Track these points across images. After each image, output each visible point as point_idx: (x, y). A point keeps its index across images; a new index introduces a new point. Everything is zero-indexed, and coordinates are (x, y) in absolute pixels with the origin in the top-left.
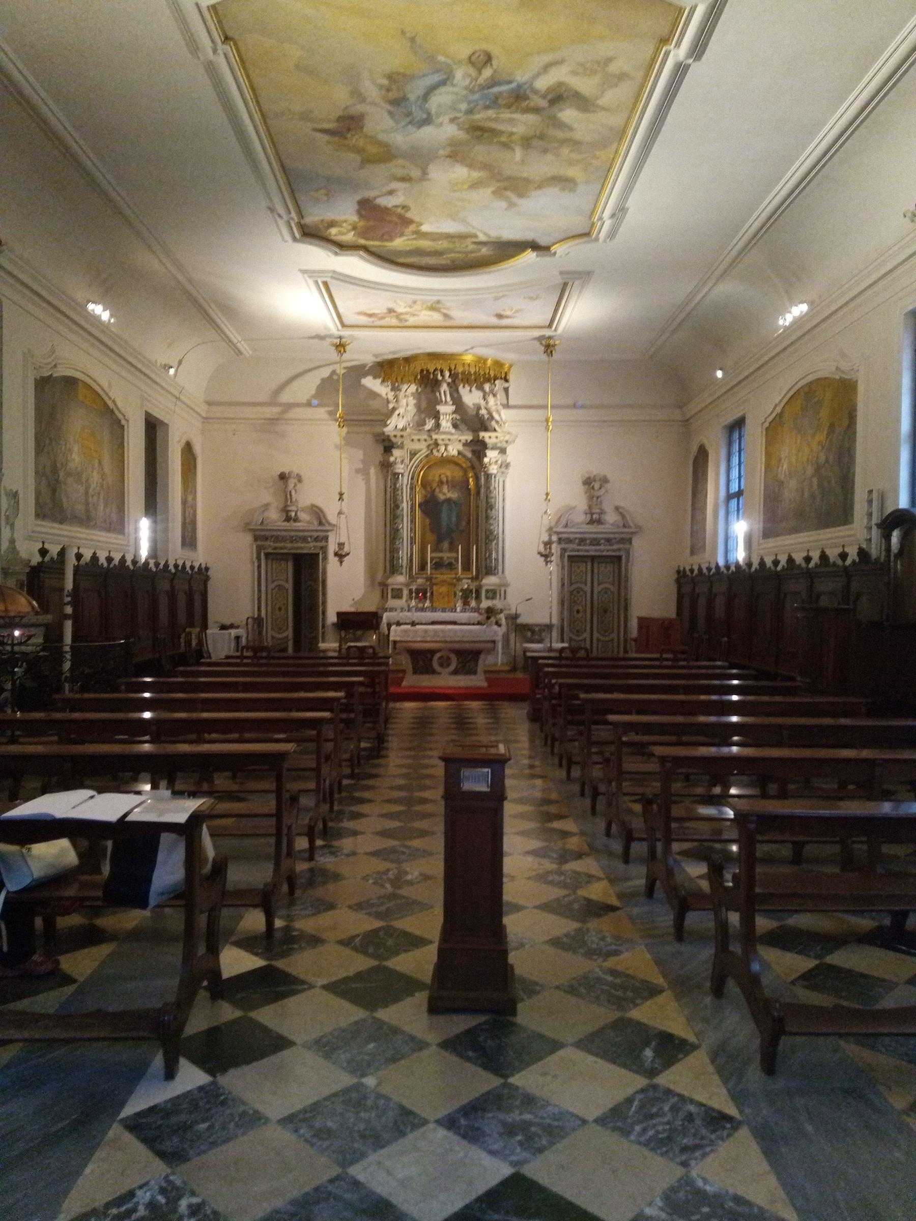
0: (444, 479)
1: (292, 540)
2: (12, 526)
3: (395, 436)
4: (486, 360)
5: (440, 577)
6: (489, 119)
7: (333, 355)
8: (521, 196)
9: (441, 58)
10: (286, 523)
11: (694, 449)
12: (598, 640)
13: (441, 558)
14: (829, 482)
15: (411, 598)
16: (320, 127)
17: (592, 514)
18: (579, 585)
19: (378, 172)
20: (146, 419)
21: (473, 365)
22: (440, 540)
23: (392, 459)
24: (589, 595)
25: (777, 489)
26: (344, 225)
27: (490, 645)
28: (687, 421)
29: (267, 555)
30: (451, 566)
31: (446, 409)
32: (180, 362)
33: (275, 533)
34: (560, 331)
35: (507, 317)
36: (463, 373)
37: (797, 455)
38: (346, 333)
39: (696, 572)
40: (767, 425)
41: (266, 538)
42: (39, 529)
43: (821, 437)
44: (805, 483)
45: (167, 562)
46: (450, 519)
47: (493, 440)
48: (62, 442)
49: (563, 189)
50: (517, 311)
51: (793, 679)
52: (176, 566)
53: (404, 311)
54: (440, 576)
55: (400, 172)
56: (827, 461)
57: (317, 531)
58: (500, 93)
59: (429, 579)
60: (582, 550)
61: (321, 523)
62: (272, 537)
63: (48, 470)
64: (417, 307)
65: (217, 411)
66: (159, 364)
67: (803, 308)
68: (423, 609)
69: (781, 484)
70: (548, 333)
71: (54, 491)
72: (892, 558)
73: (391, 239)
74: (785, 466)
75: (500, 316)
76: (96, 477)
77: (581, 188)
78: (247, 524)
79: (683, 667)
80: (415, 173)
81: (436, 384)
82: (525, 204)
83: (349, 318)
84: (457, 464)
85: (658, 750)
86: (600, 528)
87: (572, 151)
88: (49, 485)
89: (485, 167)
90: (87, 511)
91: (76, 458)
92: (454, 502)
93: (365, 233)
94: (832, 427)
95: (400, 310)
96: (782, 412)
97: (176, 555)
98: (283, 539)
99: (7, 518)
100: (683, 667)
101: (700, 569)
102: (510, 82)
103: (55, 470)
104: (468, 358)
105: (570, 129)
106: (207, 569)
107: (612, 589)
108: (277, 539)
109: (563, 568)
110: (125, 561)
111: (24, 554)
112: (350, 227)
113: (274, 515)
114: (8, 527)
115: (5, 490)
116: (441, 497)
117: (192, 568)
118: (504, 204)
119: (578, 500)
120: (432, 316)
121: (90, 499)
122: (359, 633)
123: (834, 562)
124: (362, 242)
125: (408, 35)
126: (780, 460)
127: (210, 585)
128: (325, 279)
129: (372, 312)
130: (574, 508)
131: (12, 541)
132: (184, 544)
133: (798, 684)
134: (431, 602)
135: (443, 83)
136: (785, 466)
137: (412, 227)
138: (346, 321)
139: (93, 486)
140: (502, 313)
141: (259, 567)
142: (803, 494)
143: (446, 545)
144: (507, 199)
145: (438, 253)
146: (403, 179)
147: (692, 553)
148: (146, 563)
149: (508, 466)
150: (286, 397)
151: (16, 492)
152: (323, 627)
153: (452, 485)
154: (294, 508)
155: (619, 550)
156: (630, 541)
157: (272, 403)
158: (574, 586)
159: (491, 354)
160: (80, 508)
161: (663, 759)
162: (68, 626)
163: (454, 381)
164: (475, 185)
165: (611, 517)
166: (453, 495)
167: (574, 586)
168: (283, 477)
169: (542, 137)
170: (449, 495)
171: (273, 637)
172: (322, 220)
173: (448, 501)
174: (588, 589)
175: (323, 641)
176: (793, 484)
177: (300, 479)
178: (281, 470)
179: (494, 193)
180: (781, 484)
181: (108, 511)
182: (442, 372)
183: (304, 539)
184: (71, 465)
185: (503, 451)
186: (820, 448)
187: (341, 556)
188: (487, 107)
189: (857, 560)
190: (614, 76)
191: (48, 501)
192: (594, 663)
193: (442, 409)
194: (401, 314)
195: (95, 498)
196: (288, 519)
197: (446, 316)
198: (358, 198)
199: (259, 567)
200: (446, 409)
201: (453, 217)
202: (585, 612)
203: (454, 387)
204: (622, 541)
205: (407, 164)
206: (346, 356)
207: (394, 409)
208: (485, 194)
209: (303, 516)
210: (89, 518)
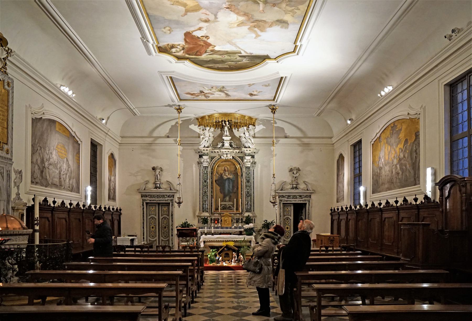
0: (227, 170)
2: (18, 187)
4: (245, 116)
5: (226, 213)
7: (176, 114)
10: (155, 189)
11: (337, 157)
13: (225, 205)
14: (406, 166)
15: (211, 223)
17: (293, 185)
18: (287, 216)
19: (193, 18)
20: (91, 142)
21: (239, 118)
22: (225, 197)
23: (202, 160)
25: (379, 171)
26: (178, 47)
27: (248, 244)
29: (147, 203)
30: (229, 208)
31: (227, 139)
32: (108, 118)
34: (278, 102)
35: (255, 95)
37: (389, 155)
38: (182, 103)
39: (340, 210)
40: (373, 142)
42: (32, 189)
43: (401, 146)
44: (394, 167)
45: (100, 206)
47: (248, 152)
48: (47, 149)
49: (282, 27)
50: (259, 92)
51: (399, 259)
52: (105, 208)
53: (207, 92)
54: (226, 213)
55: (204, 17)
56: (404, 157)
59: (220, 214)
60: (289, 201)
61: (171, 189)
62: (149, 195)
63: (39, 162)
64: (214, 90)
65: (125, 141)
66: (98, 118)
68: (217, 228)
69: (381, 169)
70: (273, 103)
71: (42, 172)
72: (444, 200)
73: (201, 55)
74: (383, 160)
75: (251, 95)
76: (65, 166)
77: (291, 27)
78: (138, 190)
79: (344, 254)
80: (211, 17)
81: (223, 127)
82: (264, 35)
83: (184, 96)
85: (316, 286)
86: (297, 191)
87: (287, 5)
88: (39, 169)
89: (245, 14)
90: (60, 182)
91: (54, 157)
92: (231, 179)
93: (188, 51)
94: (406, 141)
95: (205, 92)
96: (380, 136)
97: (105, 203)
98: (154, 196)
99: (15, 183)
100: (344, 254)
101: (342, 208)
103: (43, 162)
104: (237, 116)
106: (120, 210)
108: (151, 196)
109: (280, 209)
110: (79, 205)
111: (25, 201)
112: (181, 48)
113: (151, 186)
114: (16, 187)
115: (14, 169)
116: (225, 177)
117: (113, 209)
118: (254, 35)
119: (288, 178)
120: (220, 95)
121: (62, 176)
122: (188, 238)
123: (411, 203)
124: (187, 56)
126: (380, 158)
127: (122, 217)
128: (171, 76)
129: (193, 93)
130: (285, 182)
131: (18, 194)
132: (109, 198)
133: (401, 262)
134: (221, 224)
136: (383, 160)
137: (211, 48)
138: (182, 98)
139: (63, 170)
140: (252, 93)
141: (143, 209)
142: (392, 172)
143: (227, 198)
144: (255, 32)
145: (223, 62)
146: (207, 21)
147: (337, 202)
148: (90, 206)
149: (255, 163)
150: (155, 134)
151: (21, 171)
152: (172, 235)
153: (230, 173)
155: (305, 200)
156: (310, 196)
157: (150, 137)
159: (248, 113)
160: (56, 180)
161: (319, 290)
162: (37, 234)
163: (230, 126)
164: (241, 24)
165: (302, 186)
166: (231, 177)
168: (154, 169)
170: (229, 176)
171: (150, 240)
172: (168, 44)
173: (229, 179)
175: (313, 247)
176: (387, 168)
179: (249, 29)
180: (381, 169)
181: (71, 182)
182: (225, 122)
183: (163, 196)
184: (51, 160)
185: (253, 157)
186: (401, 151)
187: (179, 203)
189: (423, 201)
191: (39, 176)
194: (206, 93)
195: (64, 176)
196: (156, 188)
197: (227, 94)
198: (185, 32)
199: (143, 209)
201: (230, 42)
203: (230, 130)
204: (306, 196)
205: (208, 12)
206: (181, 115)
208: (245, 29)
209: (164, 186)
210: (61, 185)
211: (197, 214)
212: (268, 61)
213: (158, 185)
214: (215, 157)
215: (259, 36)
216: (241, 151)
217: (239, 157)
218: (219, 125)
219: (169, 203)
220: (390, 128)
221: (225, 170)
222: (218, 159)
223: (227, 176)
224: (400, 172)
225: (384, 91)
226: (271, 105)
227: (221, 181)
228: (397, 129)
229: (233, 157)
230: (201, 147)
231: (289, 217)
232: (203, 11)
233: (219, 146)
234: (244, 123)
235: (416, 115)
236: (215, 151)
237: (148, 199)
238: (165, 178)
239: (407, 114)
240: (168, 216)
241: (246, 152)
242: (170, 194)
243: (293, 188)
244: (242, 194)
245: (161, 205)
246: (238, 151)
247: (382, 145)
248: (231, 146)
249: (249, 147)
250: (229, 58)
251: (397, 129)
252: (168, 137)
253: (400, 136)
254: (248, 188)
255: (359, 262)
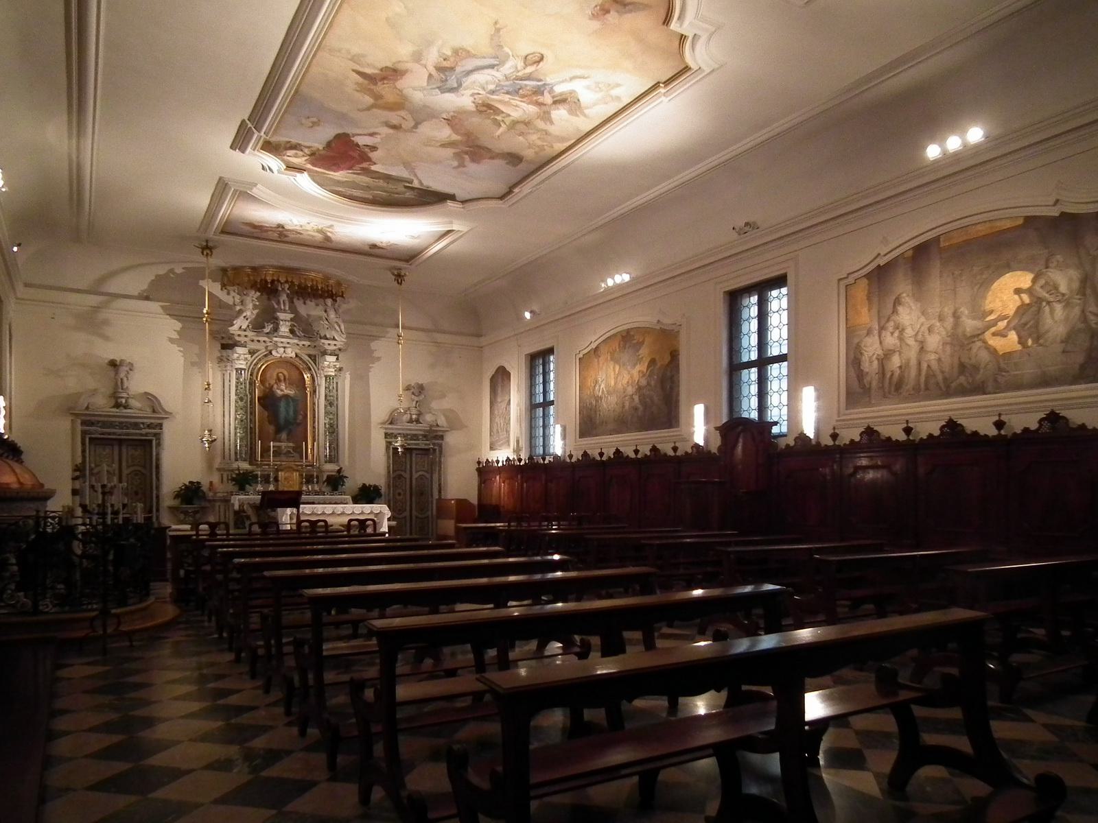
1: (122, 425)
3: (239, 335)
6: (500, 101)
8: (473, 161)
9: (506, 49)
12: (417, 517)
16: (361, 70)
24: (408, 481)
25: (594, 403)
28: (481, 347)
33: (102, 419)
36: (312, 287)
40: (581, 356)
41: (92, 424)
43: (642, 367)
46: (287, 412)
56: (648, 384)
57: (150, 418)
58: (526, 85)
61: (154, 411)
67: (626, 278)
74: (603, 386)
78: (70, 409)
84: (293, 365)
92: (291, 397)
98: (112, 425)
102: (540, 80)
105: (552, 123)
107: (143, 471)
116: (279, 392)
125: (498, 26)
135: (492, 67)
137: (365, 165)
150: (113, 287)
153: (291, 384)
154: (124, 395)
155: (146, 435)
156: (160, 426)
158: (398, 473)
166: (291, 392)
167: (398, 473)
168: (113, 364)
169: (527, 123)
170: (287, 392)
173: (286, 397)
174: (407, 476)
177: (131, 367)
178: (112, 357)
188: (508, 93)
190: (611, 96)
192: (281, 536)
193: (281, 315)
196: (117, 405)
200: (284, 316)
201: (407, 165)
202: (405, 494)
207: (241, 312)
209: (133, 402)
211: (216, 465)
212: (450, 203)
213: (124, 401)
214: (258, 351)
215: (464, 166)
216: (313, 344)
217: (310, 356)
218: (268, 289)
219: (151, 441)
220: (619, 337)
221: (279, 380)
222: (266, 356)
223: (282, 390)
224: (639, 406)
225: (613, 279)
226: (395, 268)
227: (269, 401)
228: (635, 341)
229: (297, 356)
230: (234, 329)
231: (403, 473)
232: (403, 113)
233: (267, 330)
234: (328, 291)
235: (673, 326)
236: (260, 339)
237: (97, 431)
238: (137, 384)
239: (656, 322)
240: (144, 467)
241: (327, 347)
242: (153, 421)
243: (411, 421)
244: (314, 427)
245: (415, 452)
246: (307, 343)
247: (601, 363)
248: (292, 331)
249: (334, 339)
250: (385, 185)
251: (635, 341)
252: (147, 298)
253: (641, 352)
254: (331, 417)
255: (688, 540)
